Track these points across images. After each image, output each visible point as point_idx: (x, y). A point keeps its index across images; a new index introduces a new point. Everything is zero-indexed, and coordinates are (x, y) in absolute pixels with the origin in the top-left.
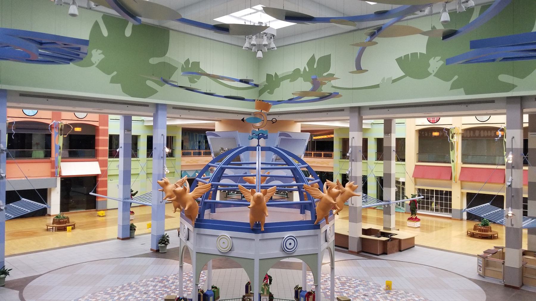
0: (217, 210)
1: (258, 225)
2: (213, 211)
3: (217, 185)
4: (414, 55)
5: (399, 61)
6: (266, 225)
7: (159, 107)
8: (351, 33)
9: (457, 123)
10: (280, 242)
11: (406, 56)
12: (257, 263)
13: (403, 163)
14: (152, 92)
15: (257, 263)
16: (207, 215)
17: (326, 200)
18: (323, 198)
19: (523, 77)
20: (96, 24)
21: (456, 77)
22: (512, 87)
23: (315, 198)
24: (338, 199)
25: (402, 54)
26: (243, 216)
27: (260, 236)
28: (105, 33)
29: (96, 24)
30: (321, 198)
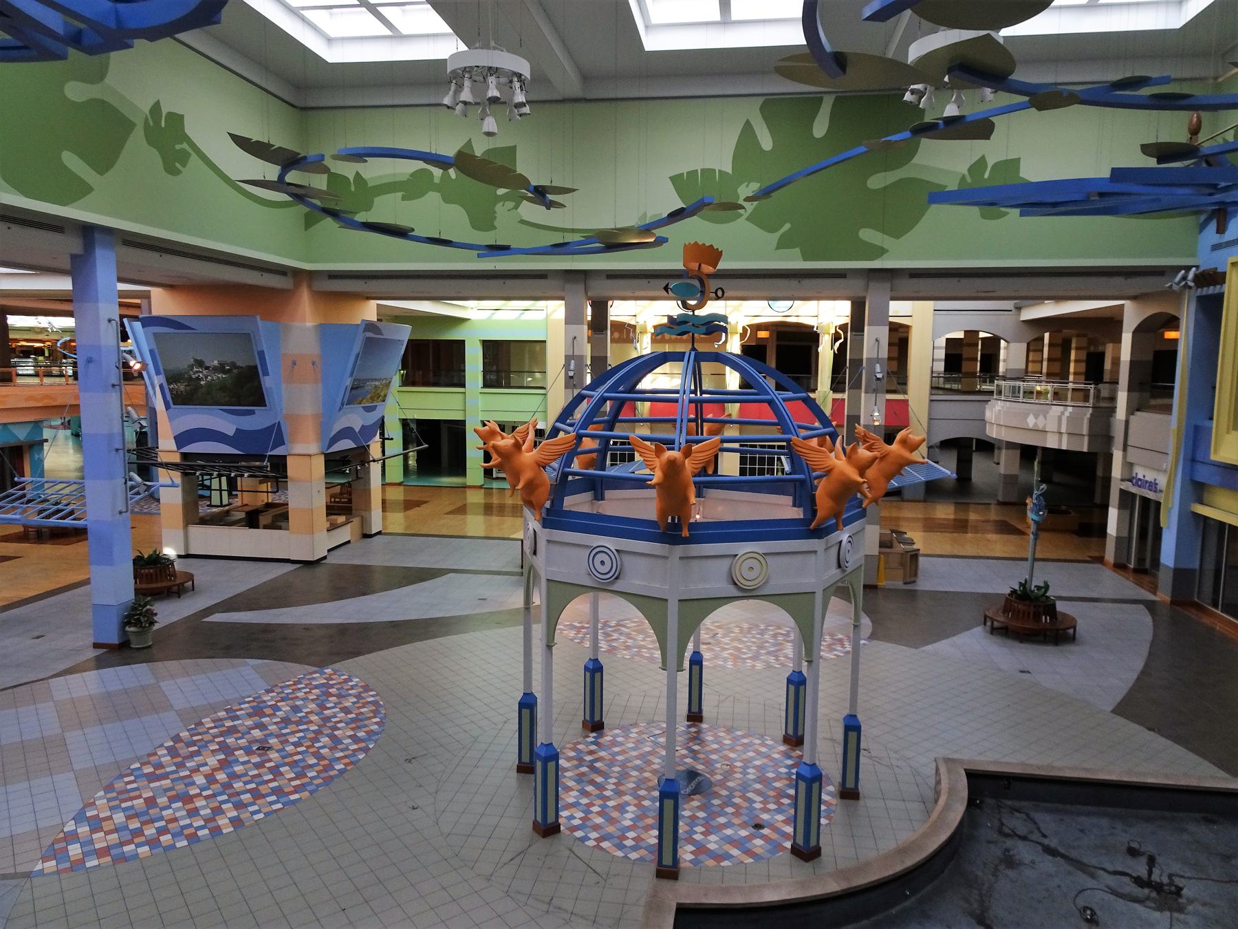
0: (609, 494)
1: (676, 527)
2: (599, 497)
3: (608, 438)
4: (708, 173)
5: (675, 180)
6: (697, 525)
7: (97, 236)
8: (568, 106)
9: (743, 314)
10: (726, 563)
11: (693, 174)
12: (673, 609)
13: (462, 390)
14: (77, 190)
15: (673, 609)
16: (577, 502)
17: (842, 473)
18: (835, 472)
19: (897, 235)
20: (748, 127)
21: (787, 226)
22: (880, 252)
23: (814, 470)
24: (870, 473)
25: (683, 168)
26: (645, 506)
27: (679, 550)
28: (766, 143)
29: (748, 127)
30: (829, 472)
